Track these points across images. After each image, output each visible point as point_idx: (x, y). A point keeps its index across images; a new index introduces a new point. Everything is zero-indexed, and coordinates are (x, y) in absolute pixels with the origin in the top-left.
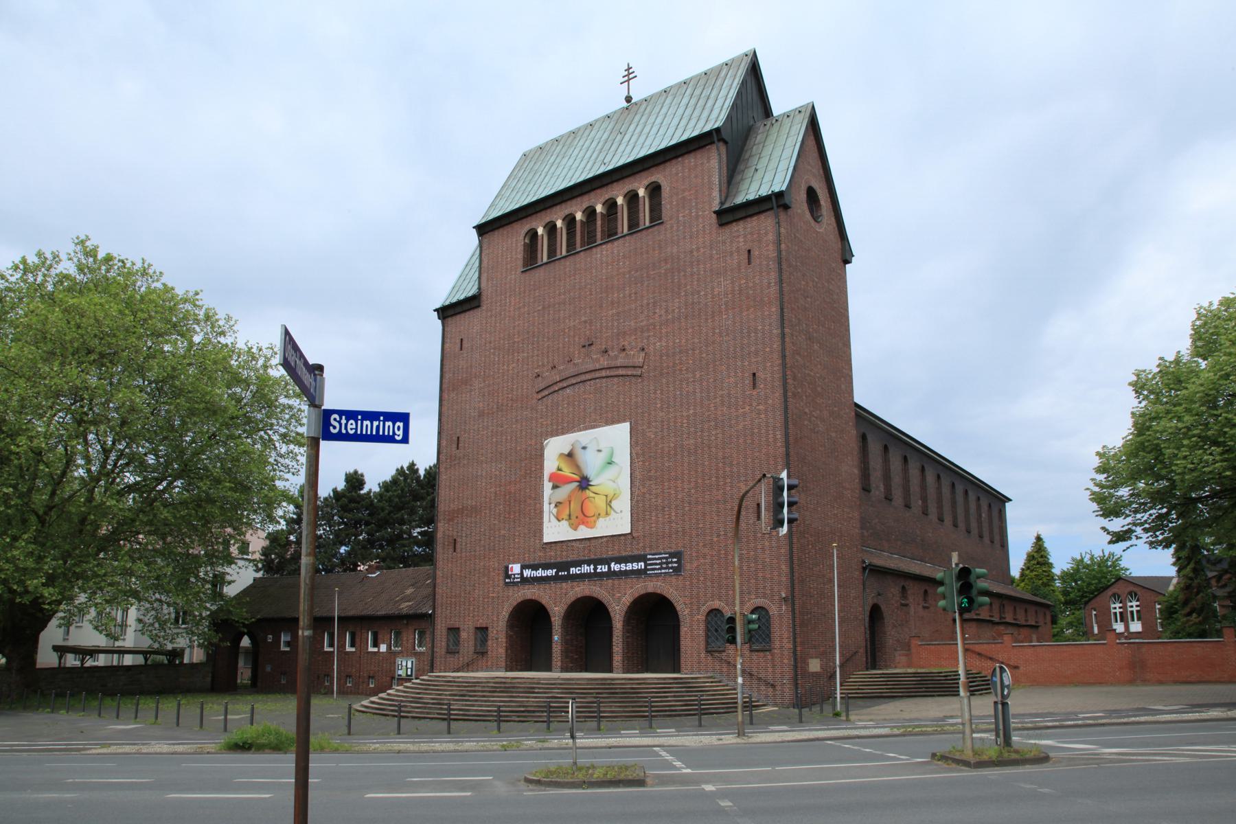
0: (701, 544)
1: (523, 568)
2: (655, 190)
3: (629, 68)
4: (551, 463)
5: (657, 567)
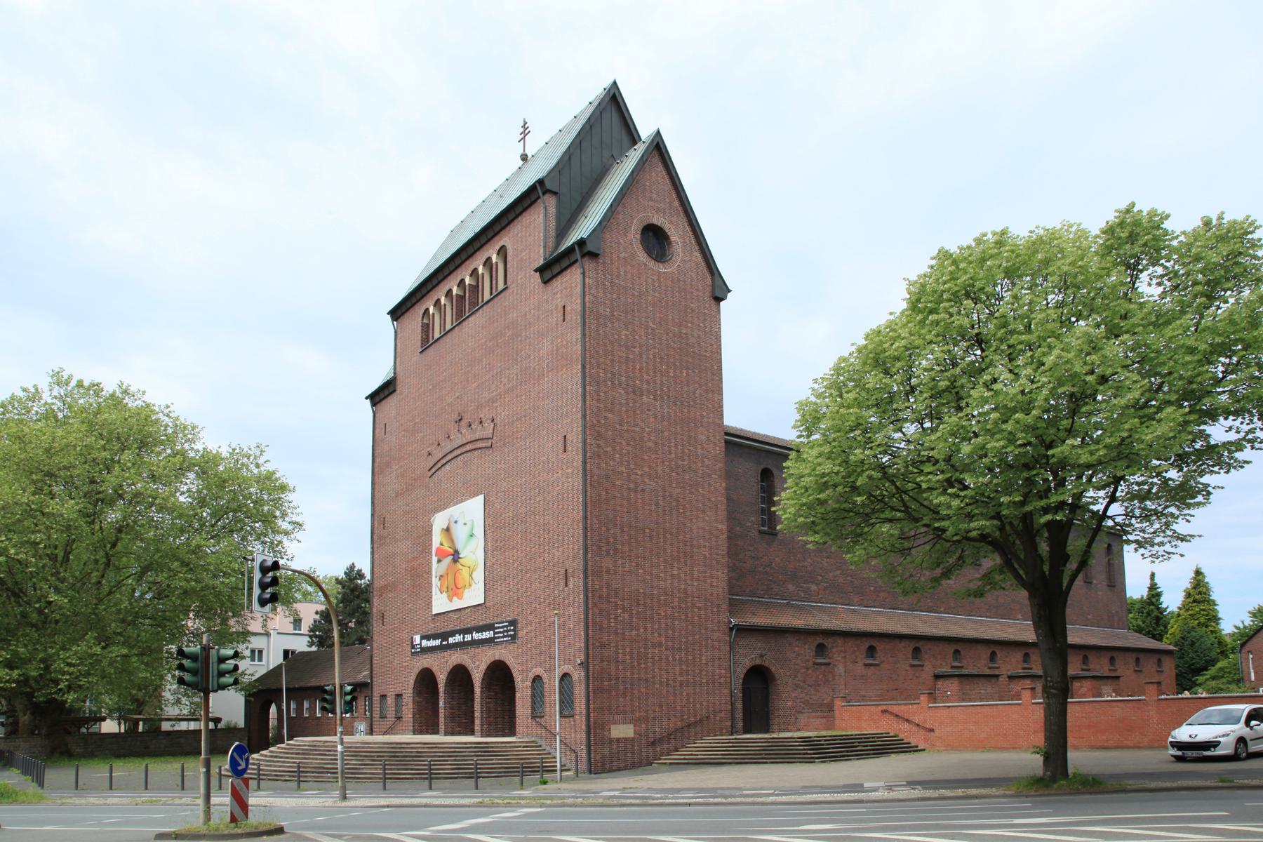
0: (529, 612)
1: (422, 638)
2: (503, 252)
3: (525, 123)
4: (437, 539)
5: (501, 635)
